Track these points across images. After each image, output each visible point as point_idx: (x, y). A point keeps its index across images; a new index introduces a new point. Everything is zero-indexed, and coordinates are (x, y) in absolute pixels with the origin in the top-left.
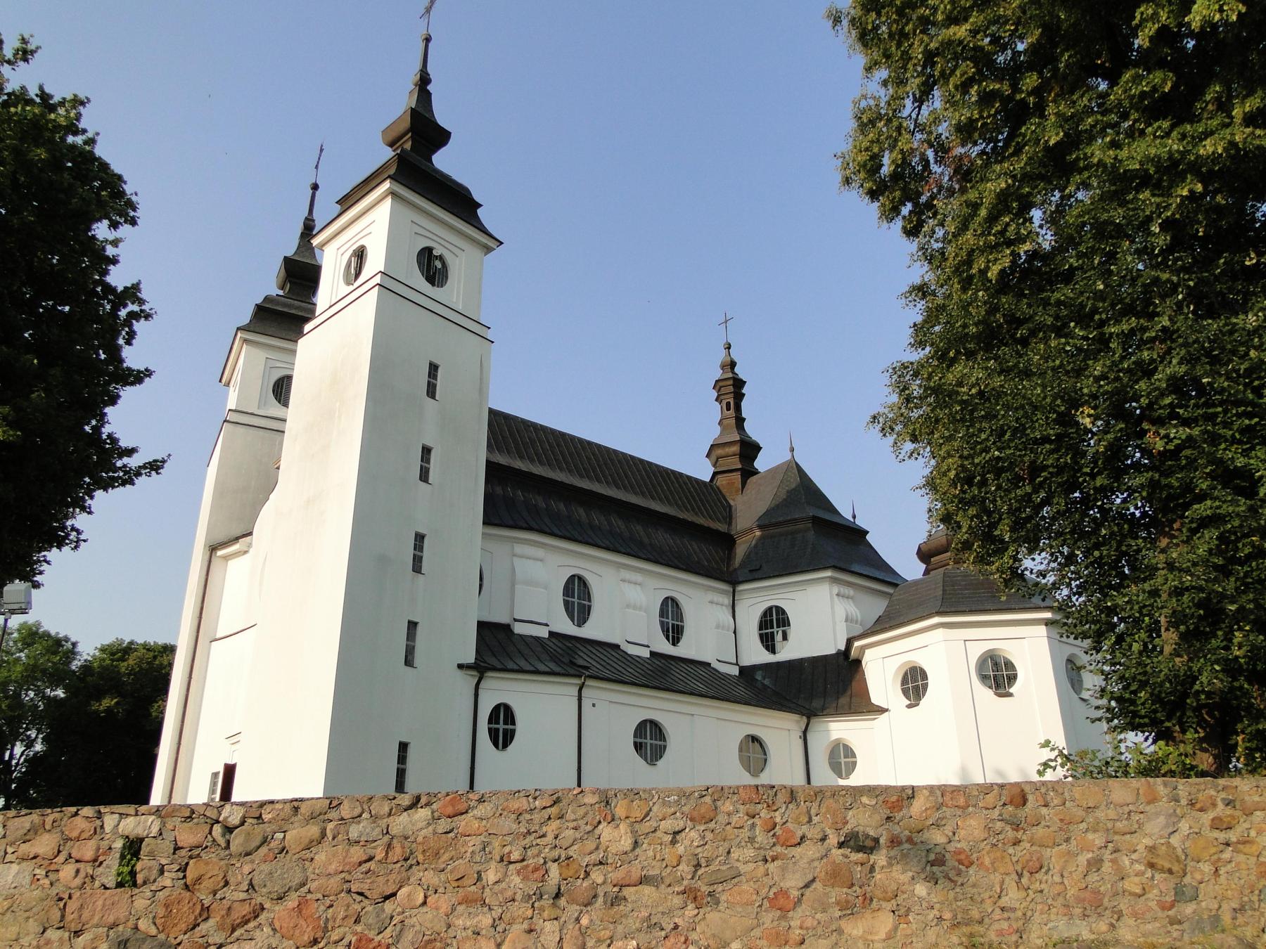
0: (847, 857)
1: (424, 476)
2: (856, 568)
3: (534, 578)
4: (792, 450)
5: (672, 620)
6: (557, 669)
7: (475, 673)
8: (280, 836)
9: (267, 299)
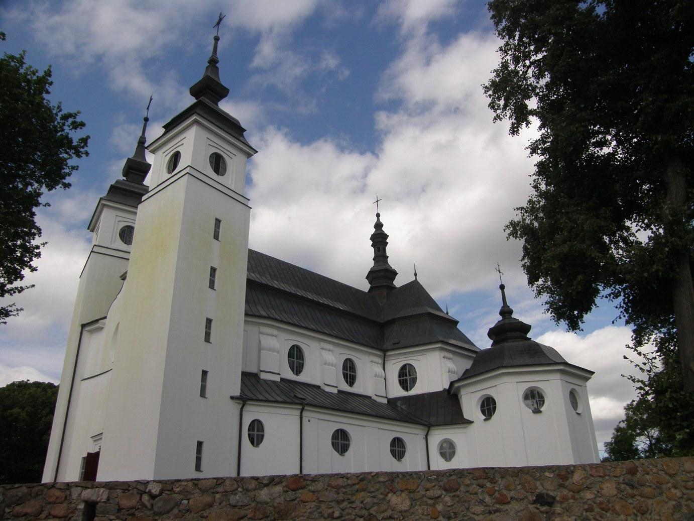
0: (538, 509)
1: (212, 285)
2: (452, 341)
3: (272, 349)
4: (416, 275)
5: (349, 372)
6: (288, 400)
7: (241, 402)
8: (185, 502)
9: (117, 182)
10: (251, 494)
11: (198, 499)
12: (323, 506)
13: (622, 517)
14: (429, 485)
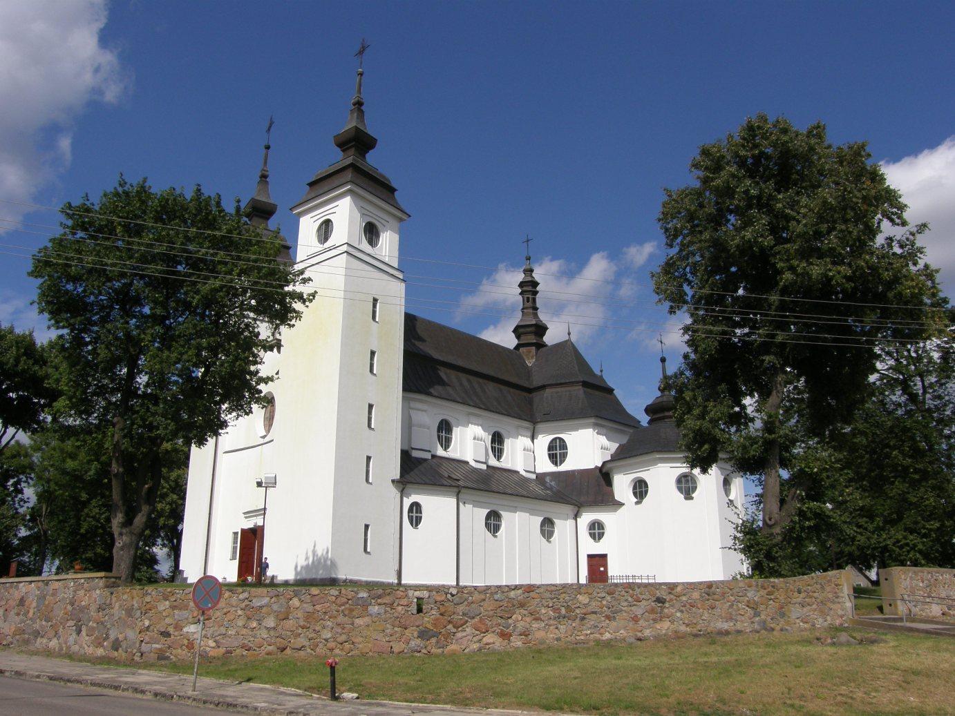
4: (569, 334)
10: (505, 594)
11: (477, 596)
12: (544, 601)
13: (701, 610)
14: (599, 591)
